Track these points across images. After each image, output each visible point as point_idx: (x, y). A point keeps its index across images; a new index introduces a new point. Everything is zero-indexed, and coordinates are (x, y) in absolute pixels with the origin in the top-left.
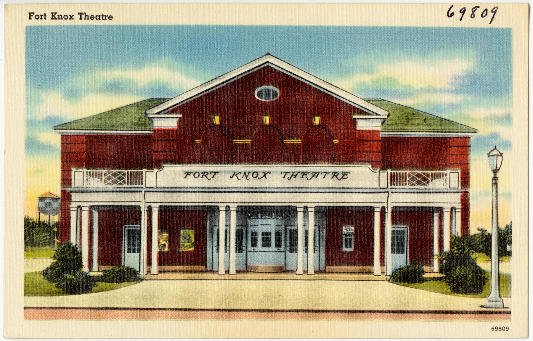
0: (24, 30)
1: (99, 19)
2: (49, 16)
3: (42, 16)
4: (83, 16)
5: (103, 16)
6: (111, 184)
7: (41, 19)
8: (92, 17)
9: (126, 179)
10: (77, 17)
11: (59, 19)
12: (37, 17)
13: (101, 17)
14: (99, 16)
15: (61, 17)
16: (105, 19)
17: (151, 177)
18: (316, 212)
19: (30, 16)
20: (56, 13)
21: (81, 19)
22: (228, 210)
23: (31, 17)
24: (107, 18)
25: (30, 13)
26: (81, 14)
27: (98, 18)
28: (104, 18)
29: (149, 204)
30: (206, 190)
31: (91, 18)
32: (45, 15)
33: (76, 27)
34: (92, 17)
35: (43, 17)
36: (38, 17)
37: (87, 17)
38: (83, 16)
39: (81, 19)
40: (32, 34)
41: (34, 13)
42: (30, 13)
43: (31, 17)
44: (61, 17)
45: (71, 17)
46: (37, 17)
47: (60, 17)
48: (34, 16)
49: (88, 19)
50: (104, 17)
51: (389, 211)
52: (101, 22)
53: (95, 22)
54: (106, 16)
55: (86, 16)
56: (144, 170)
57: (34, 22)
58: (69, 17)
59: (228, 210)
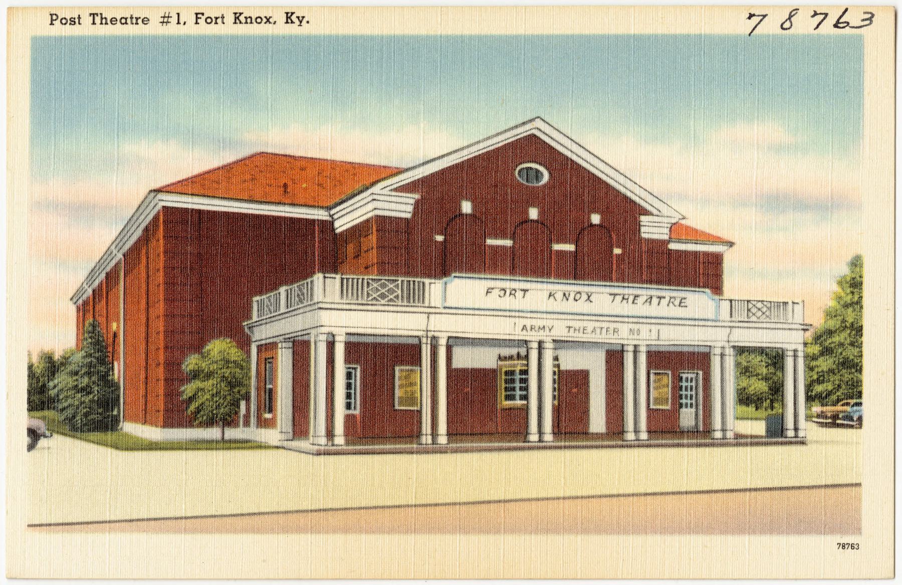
0: (28, 43)
1: (126, 23)
2: (230, 18)
3: (216, 18)
4: (98, 20)
5: (132, 18)
6: (377, 300)
7: (216, 23)
8: (113, 21)
9: (399, 292)
10: (87, 20)
11: (246, 23)
12: (209, 20)
13: (129, 21)
14: (126, 19)
15: (249, 20)
16: (137, 24)
17: (435, 288)
18: (649, 354)
19: (197, 18)
20: (241, 14)
21: (94, 23)
22: (636, 352)
23: (199, 21)
24: (140, 21)
25: (197, 14)
26: (93, 15)
27: (124, 21)
28: (134, 21)
29: (433, 333)
30: (508, 314)
31: (111, 21)
32: (223, 17)
33: (155, 38)
34: (113, 21)
35: (219, 21)
36: (209, 21)
37: (104, 21)
38: (98, 20)
39: (94, 23)
40: (42, 49)
41: (203, 14)
42: (197, 14)
43: (199, 21)
44: (249, 20)
45: (145, 21)
46: (209, 20)
47: (249, 20)
48: (204, 18)
49: (106, 23)
50: (135, 20)
51: (643, 349)
52: (130, 30)
53: (118, 30)
54: (137, 19)
55: (102, 18)
56: (427, 281)
57: (59, 30)
58: (265, 20)
59: (636, 352)
